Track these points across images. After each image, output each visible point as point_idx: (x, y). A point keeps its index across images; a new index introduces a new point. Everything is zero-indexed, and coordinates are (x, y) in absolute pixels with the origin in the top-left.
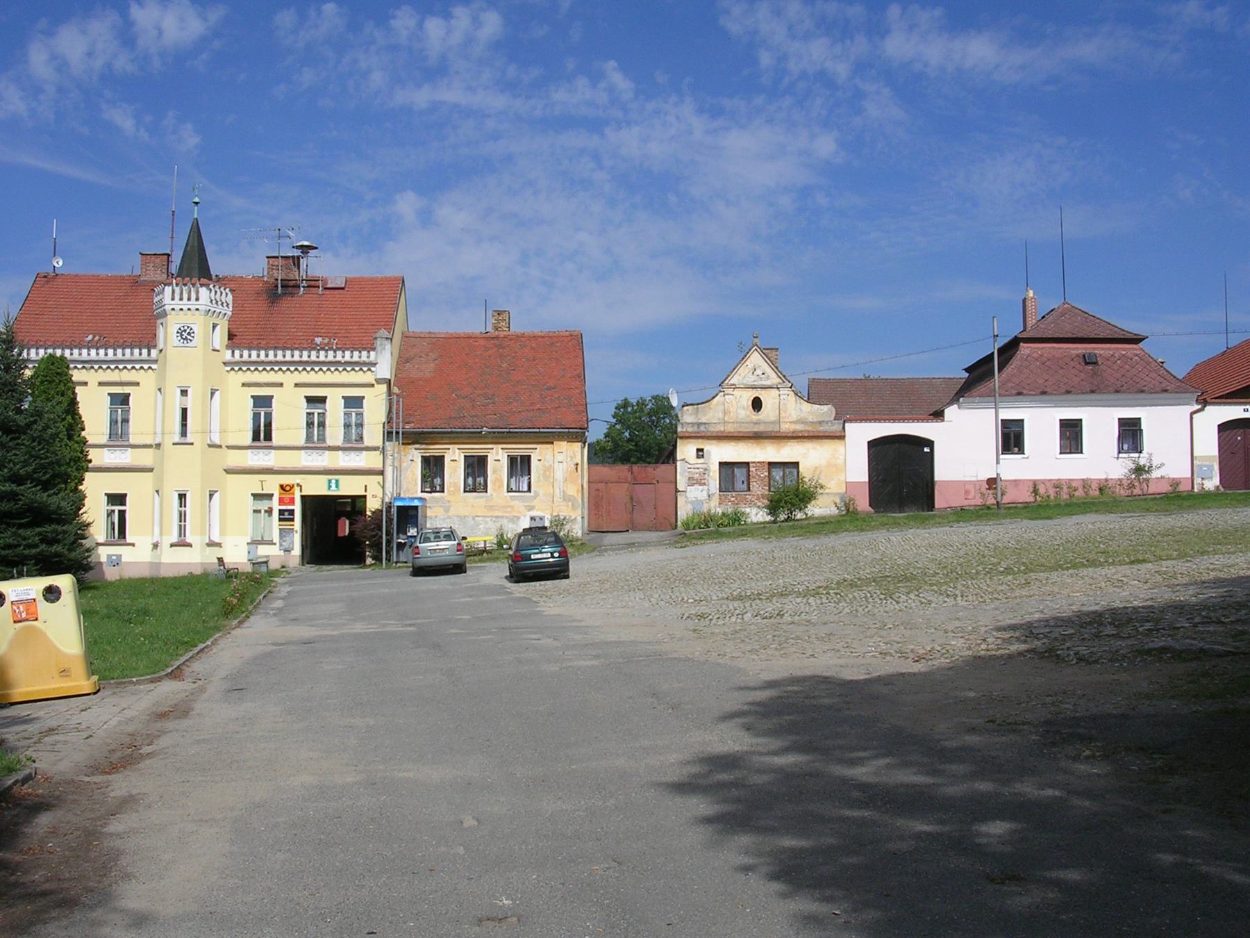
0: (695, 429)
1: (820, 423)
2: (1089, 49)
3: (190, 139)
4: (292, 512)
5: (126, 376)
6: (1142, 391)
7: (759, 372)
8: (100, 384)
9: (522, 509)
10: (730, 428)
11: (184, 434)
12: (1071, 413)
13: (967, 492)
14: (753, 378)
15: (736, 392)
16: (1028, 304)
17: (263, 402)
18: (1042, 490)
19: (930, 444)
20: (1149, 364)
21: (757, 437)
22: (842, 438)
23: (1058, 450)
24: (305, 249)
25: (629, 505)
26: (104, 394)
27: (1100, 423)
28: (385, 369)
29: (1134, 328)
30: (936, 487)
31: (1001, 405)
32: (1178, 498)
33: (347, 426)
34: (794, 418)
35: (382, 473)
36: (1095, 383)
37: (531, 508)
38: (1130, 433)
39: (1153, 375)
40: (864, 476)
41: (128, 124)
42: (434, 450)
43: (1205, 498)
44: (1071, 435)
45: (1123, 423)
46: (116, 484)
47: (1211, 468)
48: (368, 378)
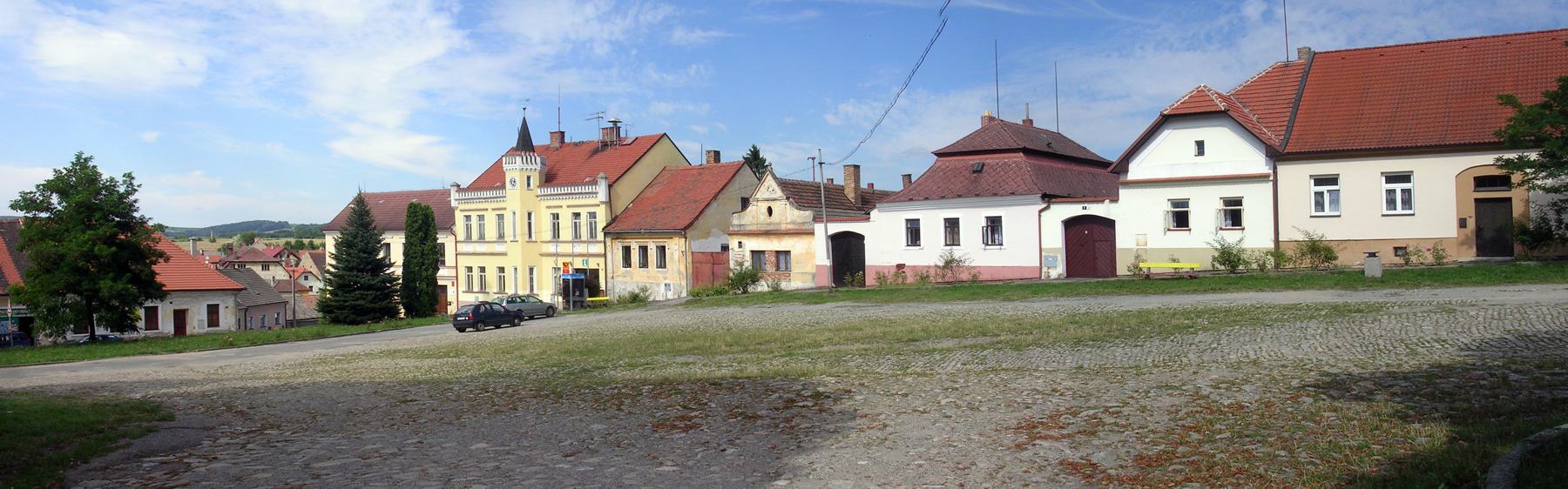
2: (714, 33)
10: (753, 228)
19: (861, 237)
21: (767, 234)
22: (812, 233)
35: (605, 255)
40: (828, 263)
42: (627, 242)
47: (1055, 259)
48: (596, 201)
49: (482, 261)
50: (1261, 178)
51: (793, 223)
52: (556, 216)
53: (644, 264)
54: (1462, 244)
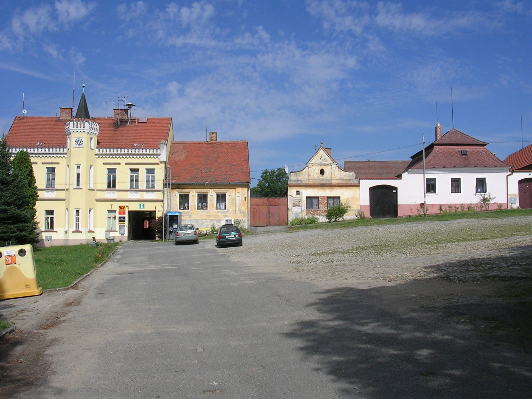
0: (296, 182)
1: (349, 180)
2: (463, 21)
3: (81, 59)
4: (124, 218)
5: (54, 160)
6: (486, 167)
7: (323, 158)
8: (43, 163)
9: (222, 217)
10: (311, 182)
11: (78, 184)
12: (456, 176)
13: (412, 209)
14: (321, 161)
15: (313, 167)
16: (438, 129)
17: (112, 171)
18: (443, 209)
19: (396, 189)
20: (489, 155)
21: (322, 186)
22: (358, 186)
23: (450, 192)
24: (130, 106)
25: (268, 215)
26: (44, 167)
27: (468, 180)
28: (164, 157)
29: (482, 139)
30: (399, 207)
31: (426, 172)
32: (501, 212)
33: (148, 181)
34: (338, 178)
35: (162, 201)
36: (466, 163)
37: (226, 216)
38: (481, 184)
39: (491, 159)
40: (368, 203)
41: (54, 53)
42: (185, 191)
43: (513, 212)
44: (456, 185)
45: (478, 180)
47: (515, 199)
48: (157, 161)
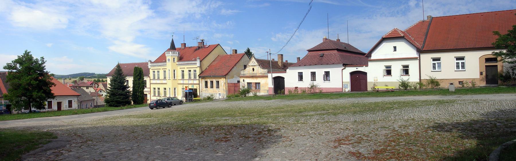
2: (235, 11)
10: (248, 75)
19: (283, 78)
21: (252, 77)
22: (267, 77)
35: (199, 84)
40: (272, 86)
42: (206, 80)
46: (59, 100)
47: (347, 85)
48: (196, 66)
49: (159, 86)
50: (415, 59)
51: (261, 73)
52: (183, 71)
53: (212, 87)
54: (481, 80)
